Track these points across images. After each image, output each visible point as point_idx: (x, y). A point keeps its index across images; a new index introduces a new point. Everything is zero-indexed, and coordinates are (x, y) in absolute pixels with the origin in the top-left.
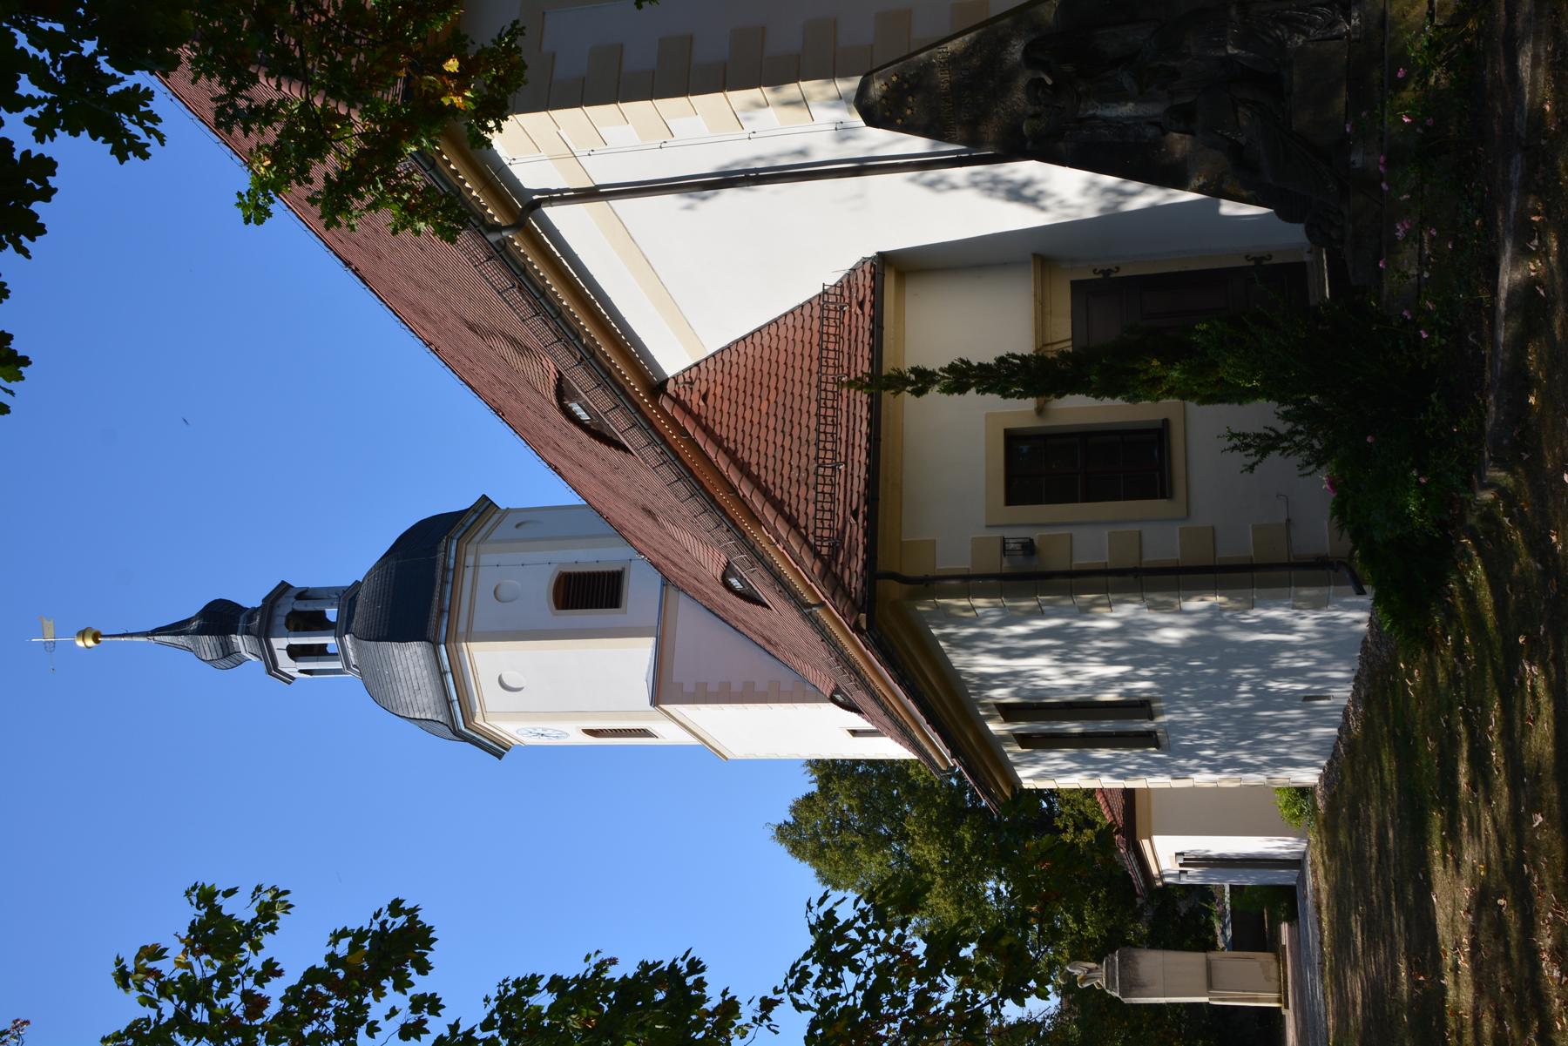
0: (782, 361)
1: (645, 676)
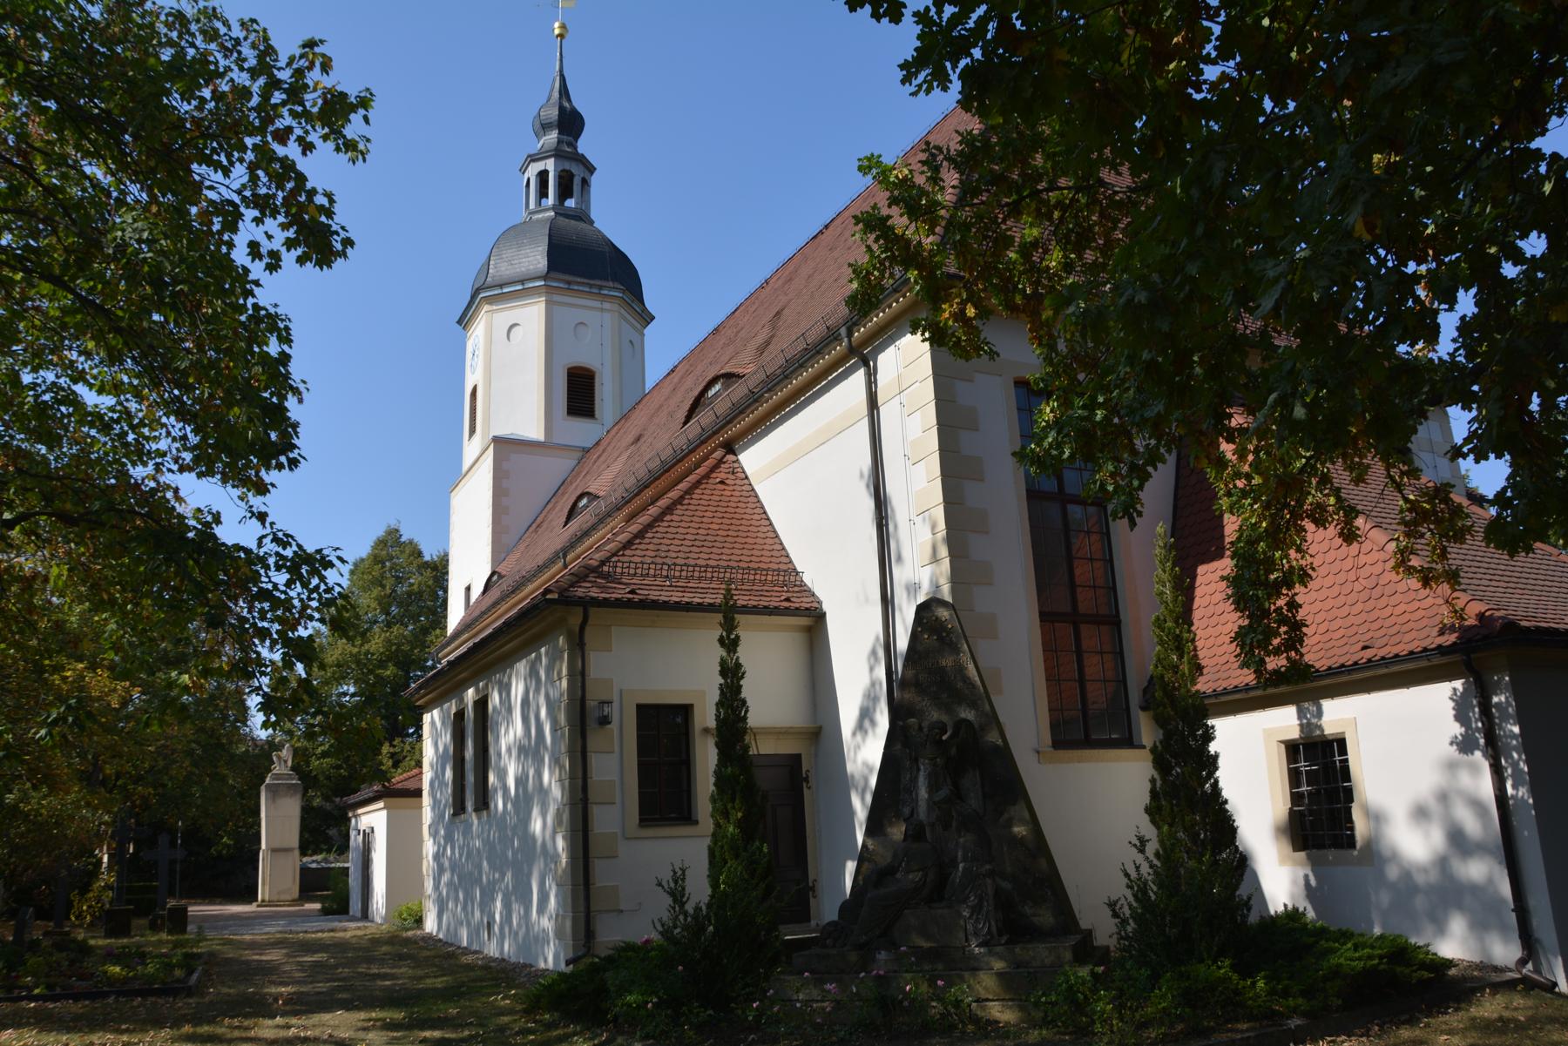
0: (748, 540)
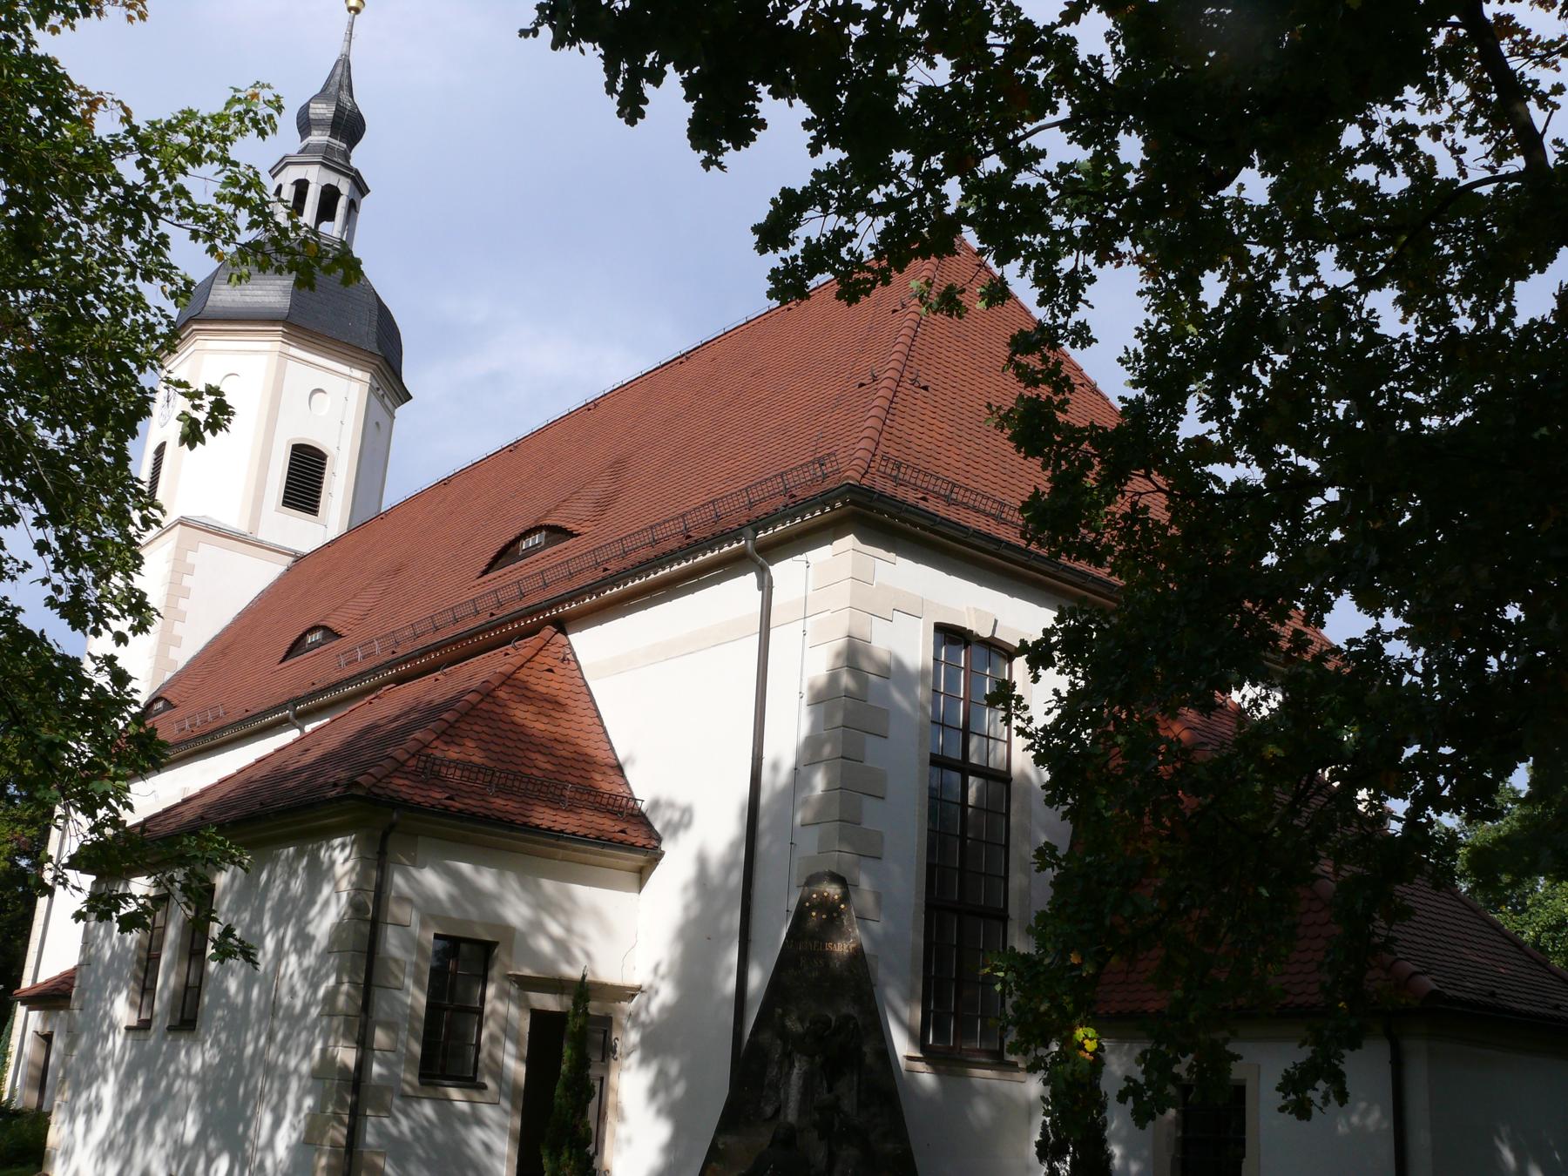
1: (209, 515)
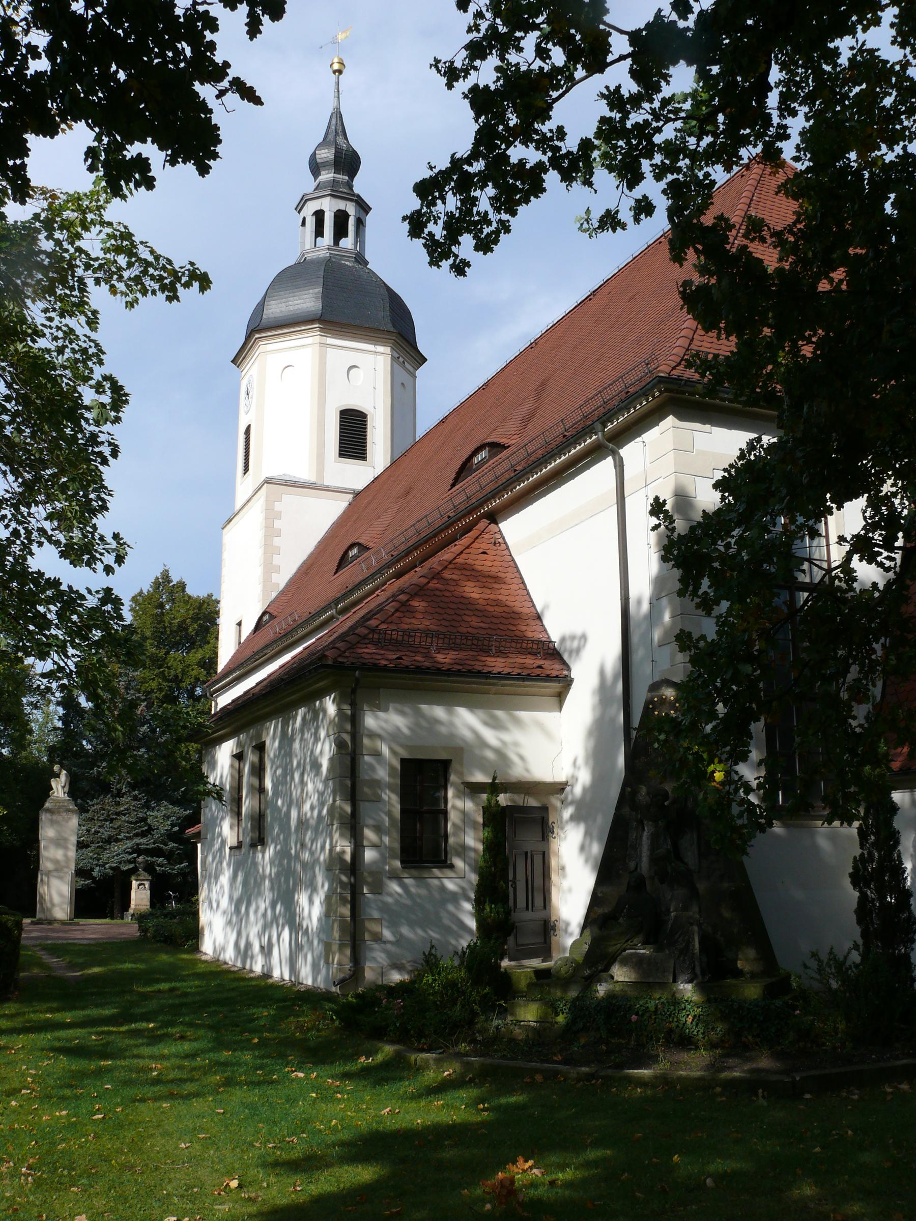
1: (287, 473)
